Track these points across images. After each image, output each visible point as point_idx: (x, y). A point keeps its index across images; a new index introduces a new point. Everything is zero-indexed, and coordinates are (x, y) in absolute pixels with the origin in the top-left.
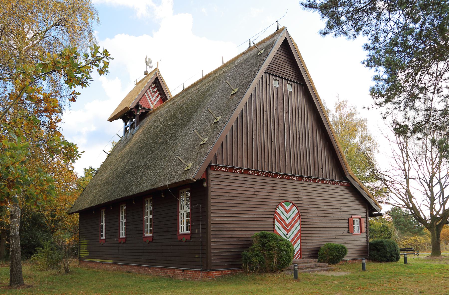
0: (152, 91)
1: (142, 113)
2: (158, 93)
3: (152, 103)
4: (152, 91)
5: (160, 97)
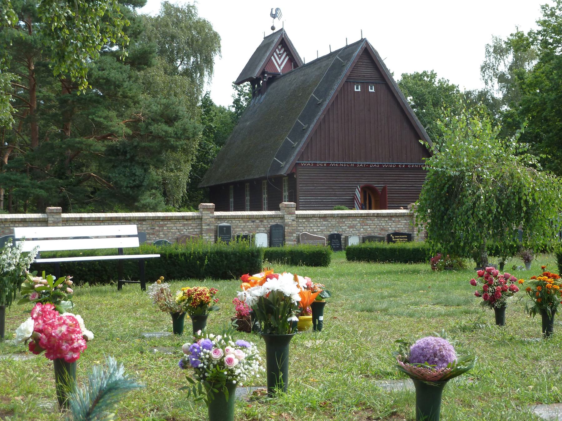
0: (278, 52)
1: (269, 78)
2: (285, 54)
3: (279, 66)
4: (278, 52)
5: (287, 58)
